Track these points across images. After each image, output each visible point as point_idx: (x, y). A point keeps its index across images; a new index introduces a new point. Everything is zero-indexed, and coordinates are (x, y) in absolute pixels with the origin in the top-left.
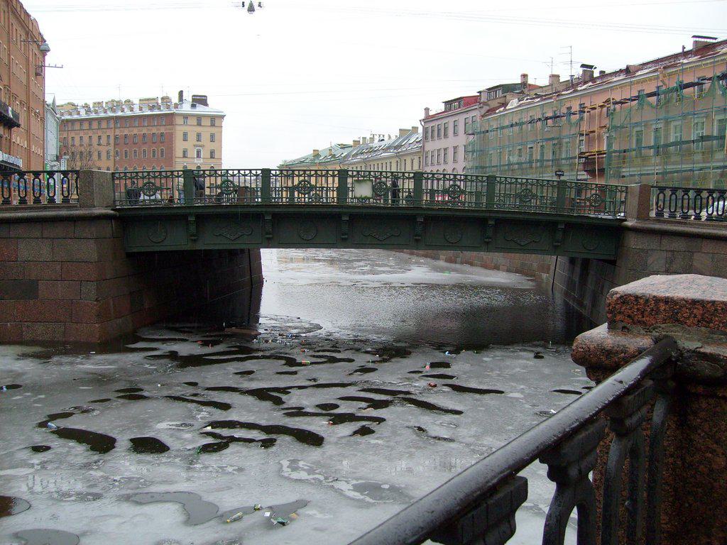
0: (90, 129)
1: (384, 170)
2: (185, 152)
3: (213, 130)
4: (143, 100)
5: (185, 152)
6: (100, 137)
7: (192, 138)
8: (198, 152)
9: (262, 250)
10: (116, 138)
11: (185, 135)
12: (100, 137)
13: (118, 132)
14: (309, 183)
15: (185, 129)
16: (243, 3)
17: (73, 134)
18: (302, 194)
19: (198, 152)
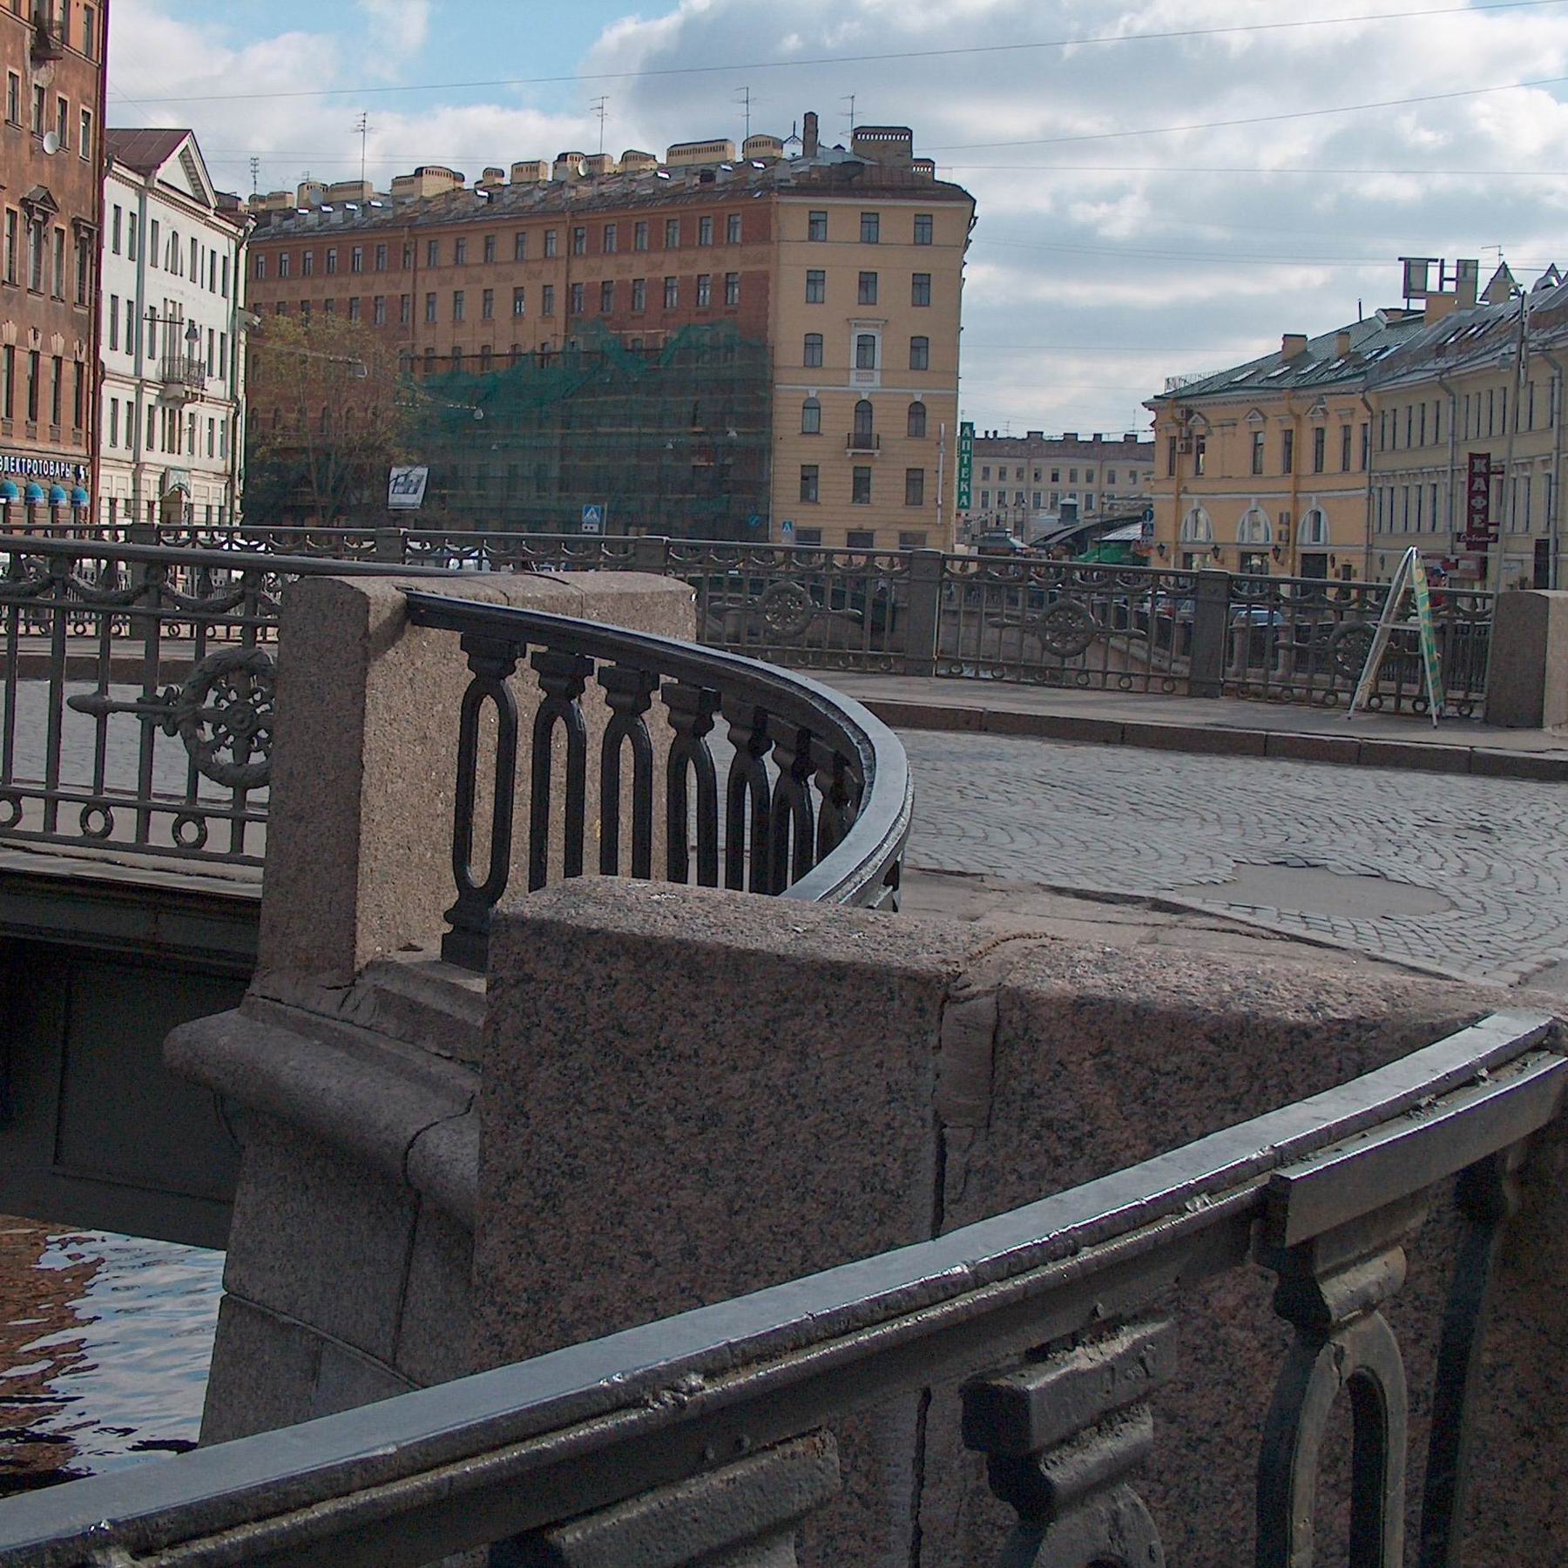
0: (518, 259)
1: (105, 521)
2: (813, 343)
3: (921, 261)
4: (755, 145)
5: (813, 343)
6: (518, 295)
7: (840, 286)
8: (865, 344)
9: (133, 841)
10: (572, 291)
11: (815, 279)
12: (518, 295)
13: (580, 274)
14: (200, 764)
15: (817, 256)
16: (83, 1414)
17: (428, 282)
18: (220, 776)
19: (865, 344)
